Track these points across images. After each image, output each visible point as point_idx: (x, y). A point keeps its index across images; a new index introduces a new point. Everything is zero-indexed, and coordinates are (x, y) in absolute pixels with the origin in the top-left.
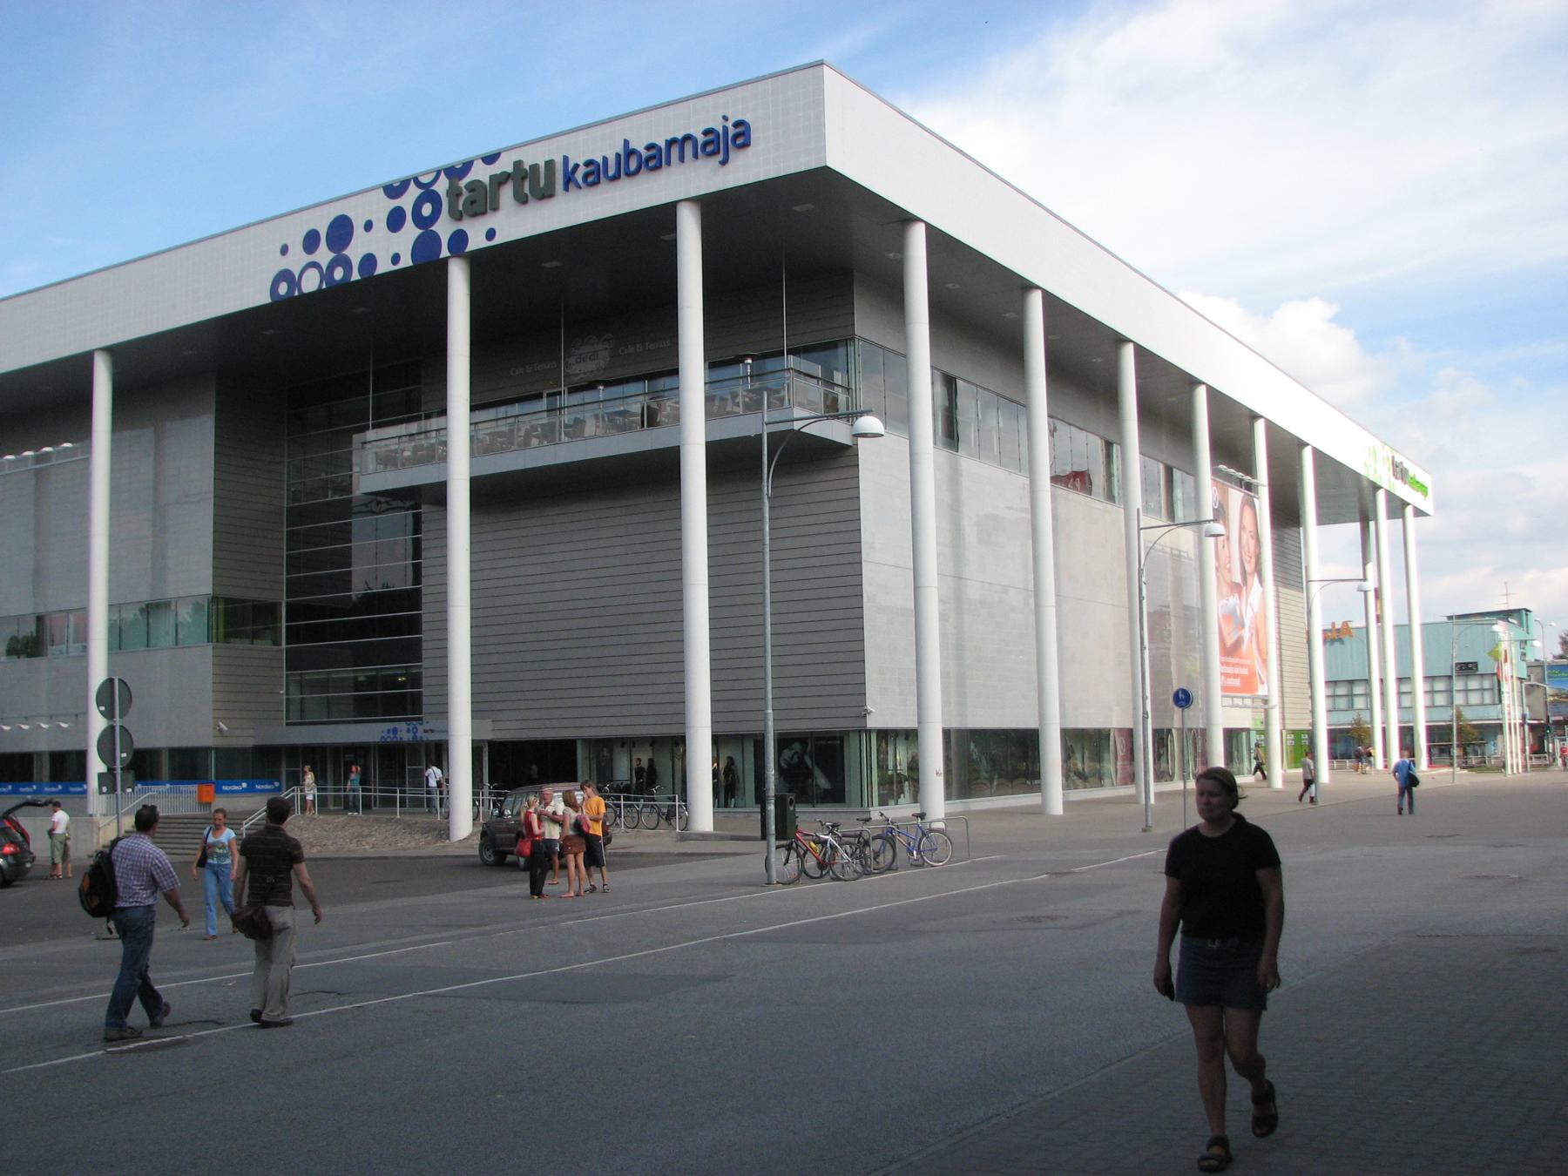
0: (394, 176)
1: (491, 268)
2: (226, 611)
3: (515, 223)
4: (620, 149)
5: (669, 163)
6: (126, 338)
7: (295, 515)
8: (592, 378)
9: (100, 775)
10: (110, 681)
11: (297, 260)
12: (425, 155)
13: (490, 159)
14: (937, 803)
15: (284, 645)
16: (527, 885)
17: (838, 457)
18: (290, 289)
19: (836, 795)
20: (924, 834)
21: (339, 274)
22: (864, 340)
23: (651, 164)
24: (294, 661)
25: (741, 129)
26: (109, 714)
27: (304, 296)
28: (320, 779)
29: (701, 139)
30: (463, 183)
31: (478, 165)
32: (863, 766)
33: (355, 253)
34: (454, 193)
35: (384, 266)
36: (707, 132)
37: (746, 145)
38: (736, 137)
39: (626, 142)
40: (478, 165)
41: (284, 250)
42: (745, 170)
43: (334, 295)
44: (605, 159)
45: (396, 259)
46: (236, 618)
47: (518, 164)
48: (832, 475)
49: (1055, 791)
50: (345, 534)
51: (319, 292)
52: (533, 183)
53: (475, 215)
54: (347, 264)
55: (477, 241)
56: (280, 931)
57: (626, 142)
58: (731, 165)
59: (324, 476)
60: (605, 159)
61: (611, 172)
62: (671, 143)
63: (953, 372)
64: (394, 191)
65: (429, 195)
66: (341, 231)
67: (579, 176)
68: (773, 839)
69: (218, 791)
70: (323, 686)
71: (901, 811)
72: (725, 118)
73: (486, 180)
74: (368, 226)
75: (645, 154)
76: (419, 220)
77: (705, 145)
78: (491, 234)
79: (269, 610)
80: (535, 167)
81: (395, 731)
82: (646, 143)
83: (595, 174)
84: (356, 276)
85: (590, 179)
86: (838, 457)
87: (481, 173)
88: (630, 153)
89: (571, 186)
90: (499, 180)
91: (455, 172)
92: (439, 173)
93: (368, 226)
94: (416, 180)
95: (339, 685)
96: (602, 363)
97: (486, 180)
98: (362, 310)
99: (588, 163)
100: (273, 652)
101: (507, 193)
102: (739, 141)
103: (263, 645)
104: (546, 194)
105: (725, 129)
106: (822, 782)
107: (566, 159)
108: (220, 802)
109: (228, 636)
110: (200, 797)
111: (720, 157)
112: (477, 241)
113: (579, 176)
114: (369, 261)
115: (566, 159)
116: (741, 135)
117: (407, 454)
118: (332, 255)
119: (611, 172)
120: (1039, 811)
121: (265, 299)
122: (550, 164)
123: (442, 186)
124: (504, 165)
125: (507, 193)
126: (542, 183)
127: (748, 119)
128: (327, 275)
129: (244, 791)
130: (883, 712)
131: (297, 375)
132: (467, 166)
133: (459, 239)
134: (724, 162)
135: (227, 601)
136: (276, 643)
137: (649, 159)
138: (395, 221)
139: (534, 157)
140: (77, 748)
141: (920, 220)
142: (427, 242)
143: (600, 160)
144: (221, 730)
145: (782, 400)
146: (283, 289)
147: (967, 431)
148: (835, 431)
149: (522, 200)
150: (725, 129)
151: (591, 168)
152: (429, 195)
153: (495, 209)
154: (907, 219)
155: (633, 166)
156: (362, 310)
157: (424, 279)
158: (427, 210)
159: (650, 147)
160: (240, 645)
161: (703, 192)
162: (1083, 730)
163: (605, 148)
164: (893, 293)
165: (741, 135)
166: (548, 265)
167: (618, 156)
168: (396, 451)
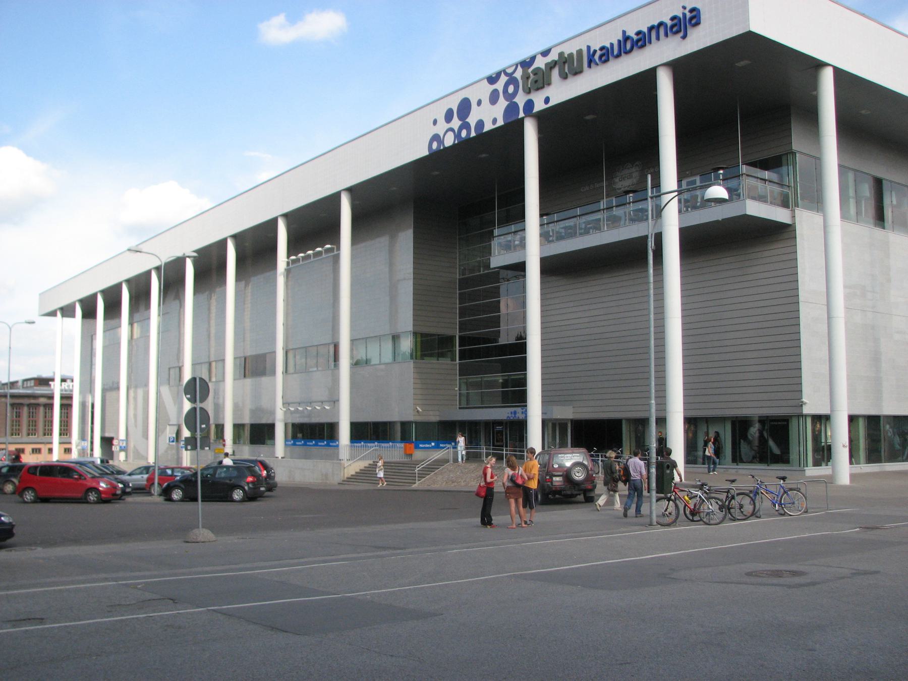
0: (492, 71)
1: (552, 121)
2: (422, 342)
3: (561, 91)
4: (620, 37)
5: (650, 42)
7: (464, 283)
8: (627, 189)
9: (186, 438)
10: (194, 380)
11: (442, 127)
12: (507, 58)
13: (545, 53)
14: (843, 469)
15: (458, 361)
16: (479, 519)
17: (777, 234)
18: (439, 146)
19: (783, 458)
20: (785, 492)
21: (464, 134)
22: (801, 153)
23: (640, 44)
24: (464, 371)
25: (694, 13)
26: (193, 400)
27: (445, 149)
28: (469, 443)
29: (669, 23)
30: (530, 70)
31: (539, 58)
32: (802, 440)
33: (472, 120)
34: (526, 77)
35: (488, 126)
36: (673, 19)
37: (698, 24)
38: (691, 19)
39: (624, 32)
40: (539, 58)
41: (435, 122)
42: (699, 40)
43: (463, 146)
44: (612, 45)
45: (495, 121)
46: (429, 345)
47: (561, 55)
48: (780, 245)
49: (843, 469)
50: (496, 293)
51: (454, 146)
52: (569, 66)
53: (538, 89)
54: (466, 126)
55: (539, 106)
57: (624, 32)
58: (688, 38)
59: (479, 259)
60: (612, 45)
61: (616, 52)
62: (651, 29)
63: (880, 175)
64: (492, 80)
65: (512, 80)
66: (465, 107)
67: (597, 57)
68: (654, 493)
69: (417, 447)
70: (478, 385)
71: (823, 471)
72: (684, 8)
73: (543, 67)
74: (479, 103)
75: (635, 38)
77: (672, 27)
78: (547, 100)
79: (451, 339)
80: (571, 55)
81: (515, 413)
82: (636, 30)
83: (606, 55)
84: (473, 134)
85: (603, 58)
86: (777, 234)
87: (540, 63)
88: (626, 38)
89: (593, 65)
90: (551, 66)
91: (525, 64)
93: (479, 103)
94: (504, 71)
95: (491, 384)
96: (635, 181)
97: (543, 67)
98: (484, 155)
99: (602, 49)
100: (451, 365)
101: (555, 73)
102: (693, 22)
103: (445, 362)
104: (578, 72)
105: (684, 15)
106: (776, 450)
107: (589, 48)
108: (418, 454)
109: (423, 356)
110: (405, 449)
111: (681, 34)
112: (539, 106)
113: (597, 57)
114: (480, 124)
115: (589, 48)
116: (694, 18)
117: (517, 243)
118: (460, 123)
119: (616, 52)
120: (829, 480)
121: (426, 153)
122: (580, 52)
123: (519, 74)
124: (553, 56)
125: (555, 73)
127: (698, 6)
128: (458, 135)
129: (433, 447)
130: (812, 404)
131: (449, 199)
132: (533, 59)
133: (529, 104)
134: (684, 37)
135: (422, 335)
136: (453, 359)
137: (638, 41)
138: (494, 98)
139: (570, 49)
140: (270, 422)
141: (827, 65)
142: (512, 108)
143: (608, 46)
144: (418, 411)
145: (739, 195)
146: (435, 146)
147: (888, 213)
148: (780, 215)
149: (564, 76)
150: (684, 15)
151: (604, 51)
152: (512, 80)
153: (549, 84)
154: (819, 65)
155: (628, 46)
156: (484, 155)
157: (512, 132)
158: (511, 89)
159: (638, 33)
160: (432, 362)
161: (671, 59)
163: (611, 38)
164: (812, 115)
165: (694, 18)
166: (588, 118)
167: (619, 41)
168: (510, 241)
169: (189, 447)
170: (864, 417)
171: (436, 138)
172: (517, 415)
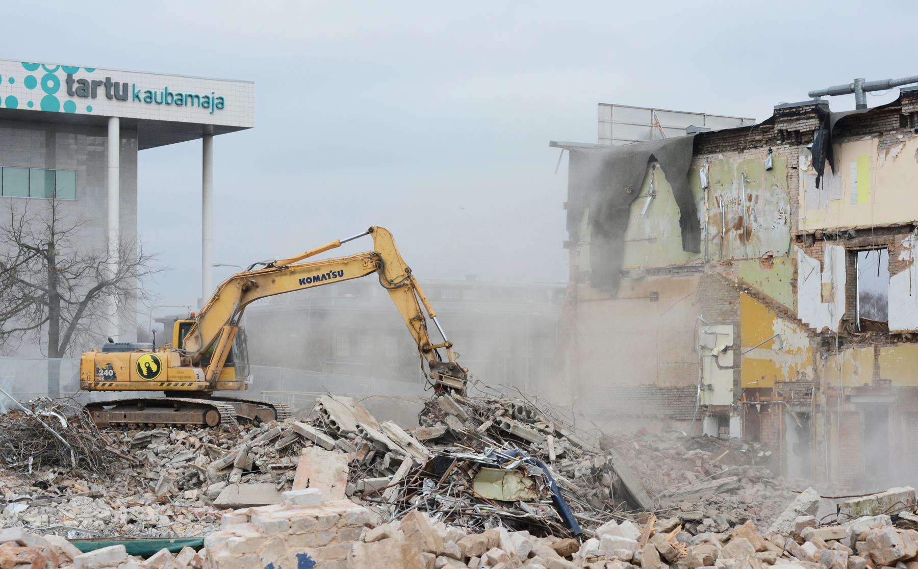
6: (157, 119)
56: (576, 153)
65: (50, 75)
76: (45, 87)
83: (150, 97)
92: (58, 67)
94: (43, 65)
104: (124, 99)
116: (221, 104)
126: (121, 93)
132: (76, 69)
149: (109, 97)
162: (681, 221)
163: (158, 88)
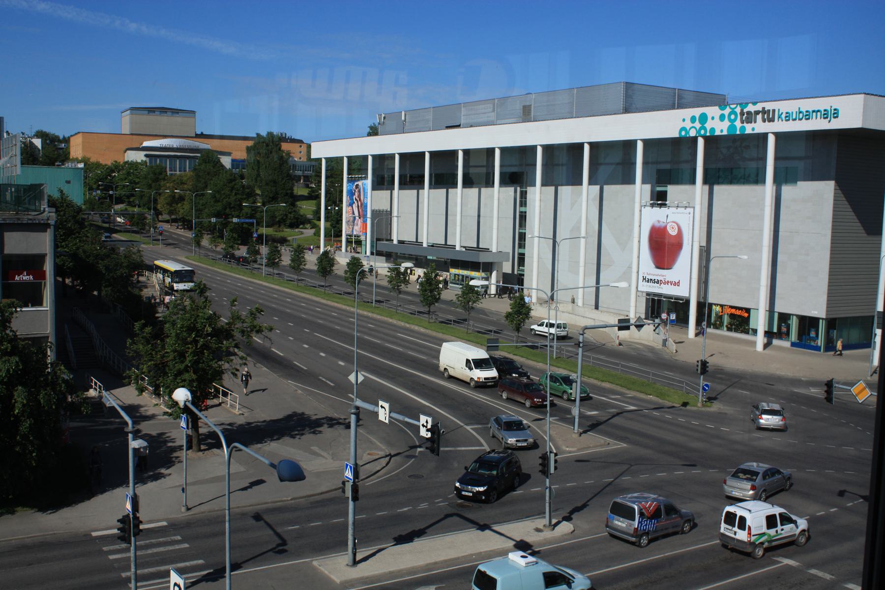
35: (717, 133)
41: (684, 120)
45: (722, 131)
81: (703, 118)
101: (759, 117)
104: (771, 120)
121: (677, 135)
125: (759, 117)
146: (683, 133)
169: (38, 142)
170: (797, 316)
171: (683, 129)
172: (709, 125)
